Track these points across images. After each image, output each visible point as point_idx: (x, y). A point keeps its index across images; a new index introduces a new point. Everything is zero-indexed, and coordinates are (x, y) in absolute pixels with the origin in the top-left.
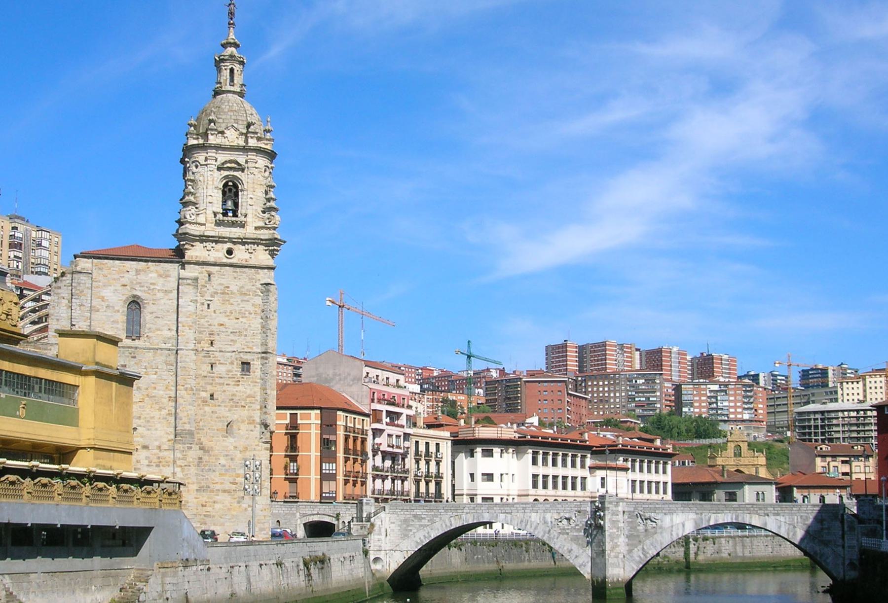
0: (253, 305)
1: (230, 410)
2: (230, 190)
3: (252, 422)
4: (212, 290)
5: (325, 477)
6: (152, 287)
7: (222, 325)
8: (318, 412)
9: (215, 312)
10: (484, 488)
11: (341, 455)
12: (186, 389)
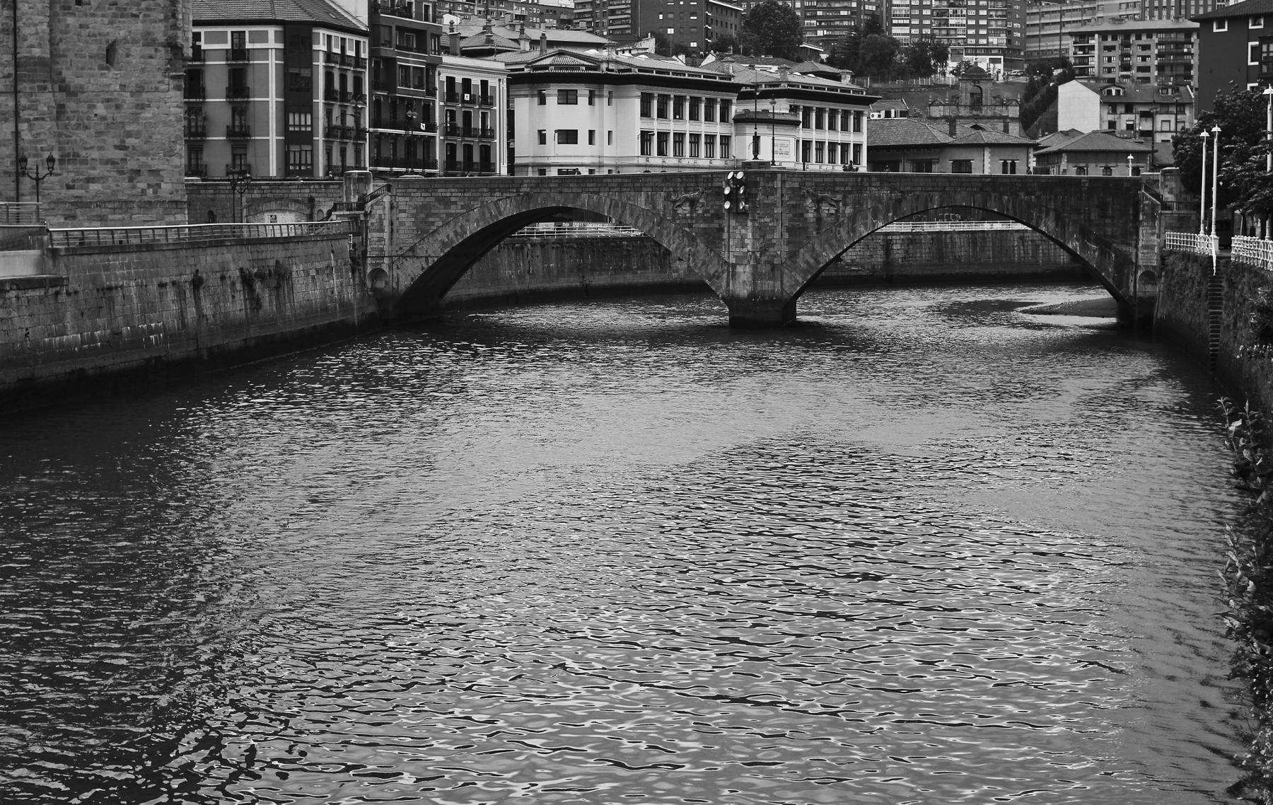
1: (111, 23)
3: (149, 41)
5: (294, 139)
8: (279, 29)
10: (559, 154)
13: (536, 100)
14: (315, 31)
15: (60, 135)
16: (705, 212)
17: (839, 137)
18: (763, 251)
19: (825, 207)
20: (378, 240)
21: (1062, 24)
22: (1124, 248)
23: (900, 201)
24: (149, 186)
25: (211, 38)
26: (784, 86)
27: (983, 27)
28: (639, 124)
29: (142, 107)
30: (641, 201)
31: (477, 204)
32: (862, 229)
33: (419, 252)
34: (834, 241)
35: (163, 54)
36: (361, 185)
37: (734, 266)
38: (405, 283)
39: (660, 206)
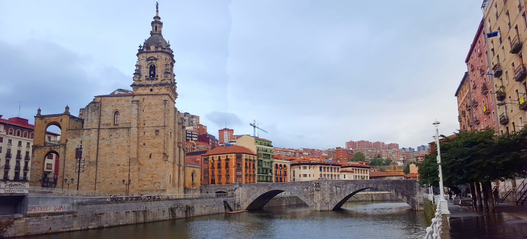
3: (159, 153)
4: (144, 105)
5: (238, 176)
10: (304, 179)
11: (244, 169)
18: (323, 200)
25: (222, 157)
28: (320, 173)
29: (157, 168)
30: (295, 188)
35: (162, 155)
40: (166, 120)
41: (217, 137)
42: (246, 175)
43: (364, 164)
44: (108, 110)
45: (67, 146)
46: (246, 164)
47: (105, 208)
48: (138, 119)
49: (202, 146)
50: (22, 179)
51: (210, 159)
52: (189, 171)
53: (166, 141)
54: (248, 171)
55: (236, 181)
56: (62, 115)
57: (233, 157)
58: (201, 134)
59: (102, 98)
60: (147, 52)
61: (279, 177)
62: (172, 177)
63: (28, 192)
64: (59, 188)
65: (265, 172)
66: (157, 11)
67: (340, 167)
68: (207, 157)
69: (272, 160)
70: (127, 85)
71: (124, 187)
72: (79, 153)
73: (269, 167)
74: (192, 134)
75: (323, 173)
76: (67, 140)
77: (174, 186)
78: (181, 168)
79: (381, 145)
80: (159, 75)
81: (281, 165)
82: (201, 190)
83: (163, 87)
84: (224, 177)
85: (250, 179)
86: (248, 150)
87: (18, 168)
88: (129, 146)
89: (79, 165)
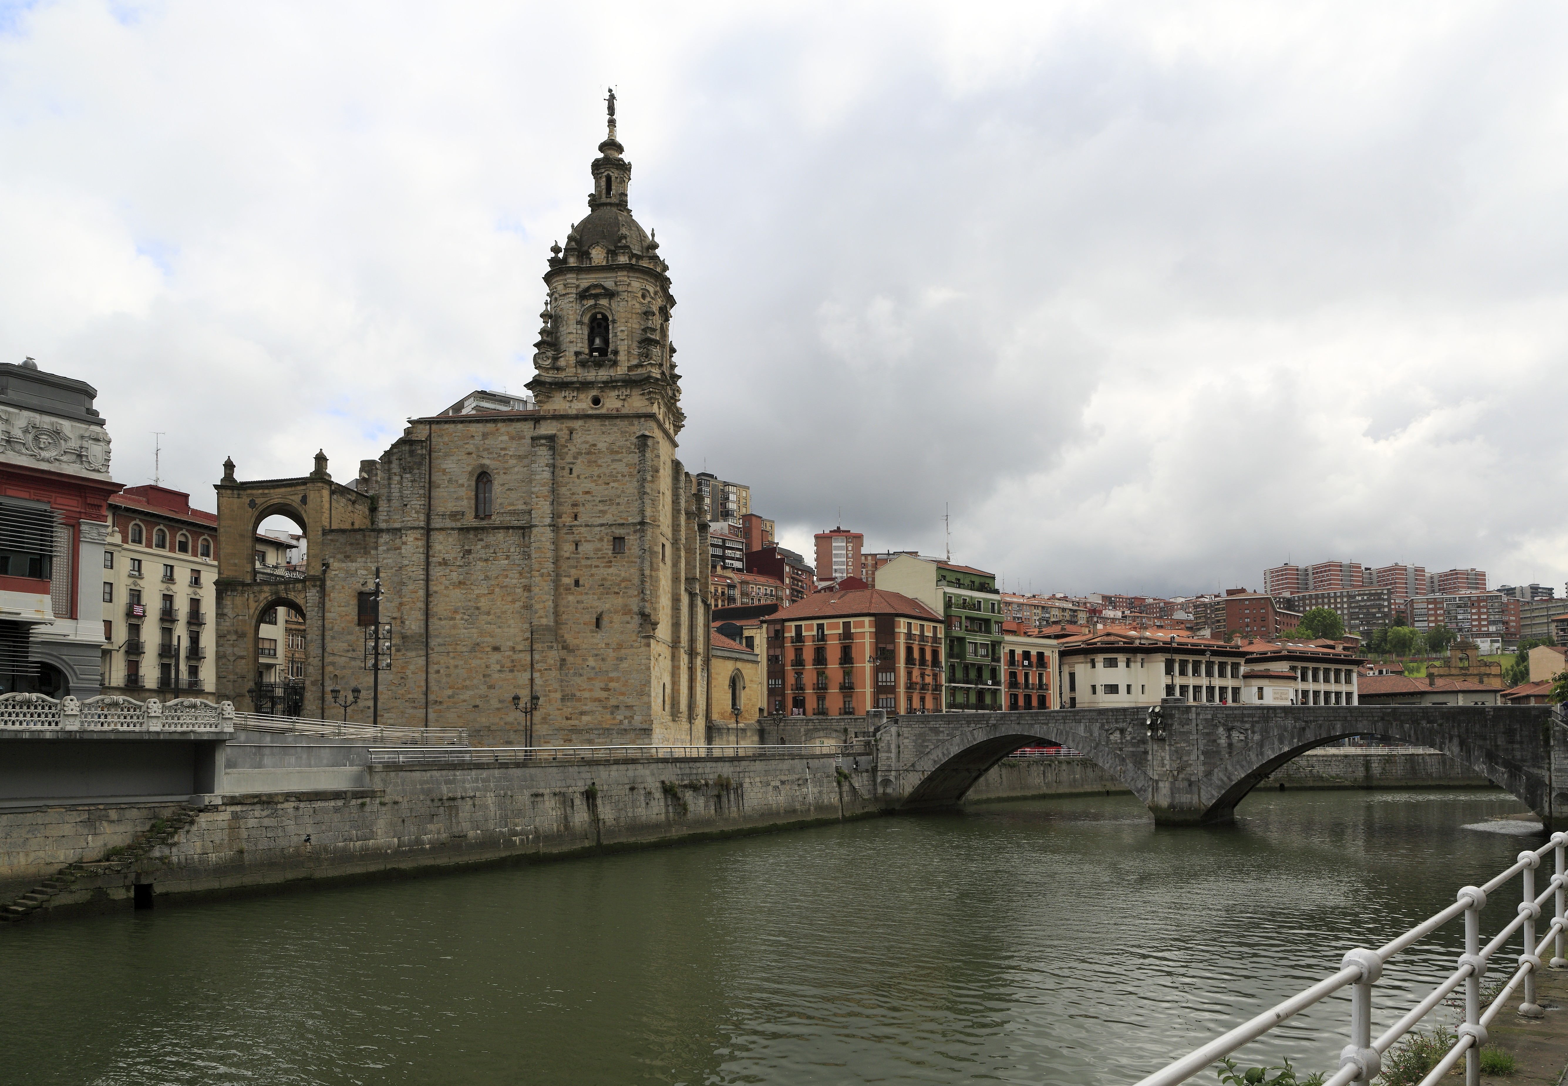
0: (627, 465)
1: (599, 599)
2: (599, 325)
4: (574, 450)
5: (882, 690)
6: (503, 453)
7: (587, 493)
8: (872, 619)
9: (578, 477)
12: (542, 575)
13: (1089, 665)
14: (897, 619)
15: (562, 681)
16: (1133, 738)
17: (1333, 687)
18: (1180, 770)
19: (1235, 734)
20: (886, 759)
21: (1548, 616)
22: (1536, 771)
23: (1304, 729)
24: (625, 718)
25: (831, 627)
26: (1285, 653)
27: (1484, 620)
28: (1165, 680)
29: (621, 659)
30: (1081, 730)
31: (958, 733)
32: (1270, 752)
33: (918, 768)
34: (1244, 763)
35: (637, 620)
36: (876, 720)
37: (1157, 782)
38: (908, 790)
39: (1096, 734)
40: (647, 501)
41: (810, 560)
42: (910, 686)
43: (1339, 649)
44: (454, 469)
45: (329, 583)
46: (909, 650)
47: (467, 782)
48: (555, 501)
49: (760, 589)
50: (185, 687)
51: (791, 633)
52: (723, 670)
53: (647, 572)
54: (916, 673)
55: (876, 704)
56: (302, 481)
57: (865, 629)
58: (756, 547)
59: (434, 427)
60: (578, 270)
61: (1021, 693)
62: (668, 691)
63: (232, 730)
64: (312, 716)
65: (973, 674)
66: (612, 123)
67: (1242, 661)
68: (778, 627)
69: (995, 635)
70: (512, 374)
71: (516, 717)
72: (367, 608)
73: (987, 661)
74: (724, 547)
75: (1179, 681)
76: (326, 565)
77: (675, 714)
78: (699, 661)
79: (1411, 576)
80: (622, 348)
81: (1026, 655)
82: (762, 734)
83: (636, 392)
84: (834, 690)
85: (923, 699)
86: (914, 603)
87: (167, 651)
88: (527, 588)
89: (376, 647)
